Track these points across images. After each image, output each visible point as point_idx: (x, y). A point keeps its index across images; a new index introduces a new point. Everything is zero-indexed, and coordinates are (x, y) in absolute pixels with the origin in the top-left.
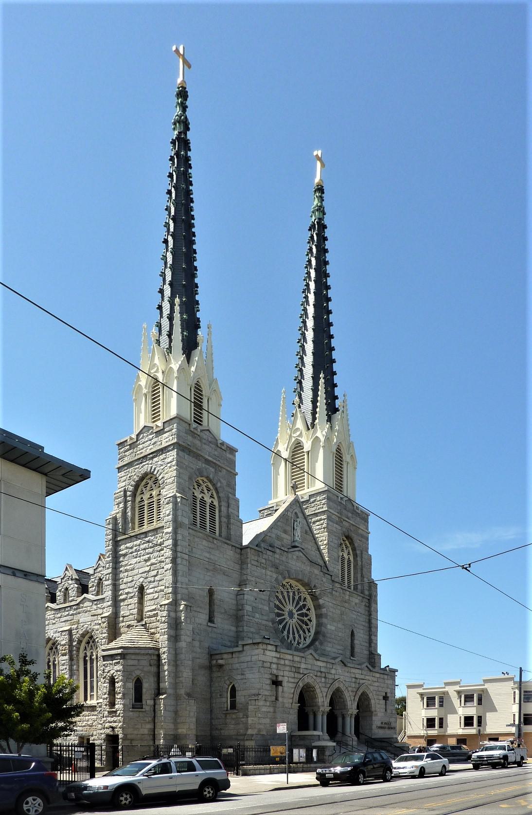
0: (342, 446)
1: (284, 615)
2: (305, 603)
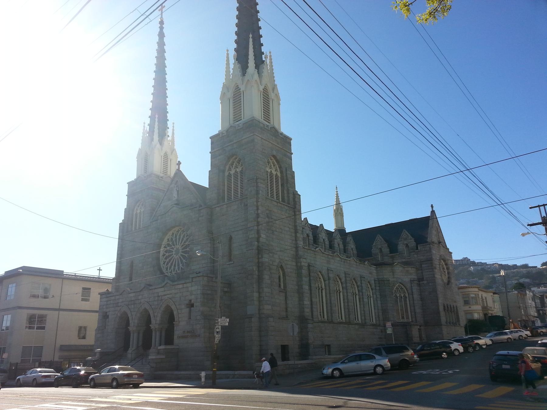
0: (268, 86)
1: (182, 255)
2: (165, 260)
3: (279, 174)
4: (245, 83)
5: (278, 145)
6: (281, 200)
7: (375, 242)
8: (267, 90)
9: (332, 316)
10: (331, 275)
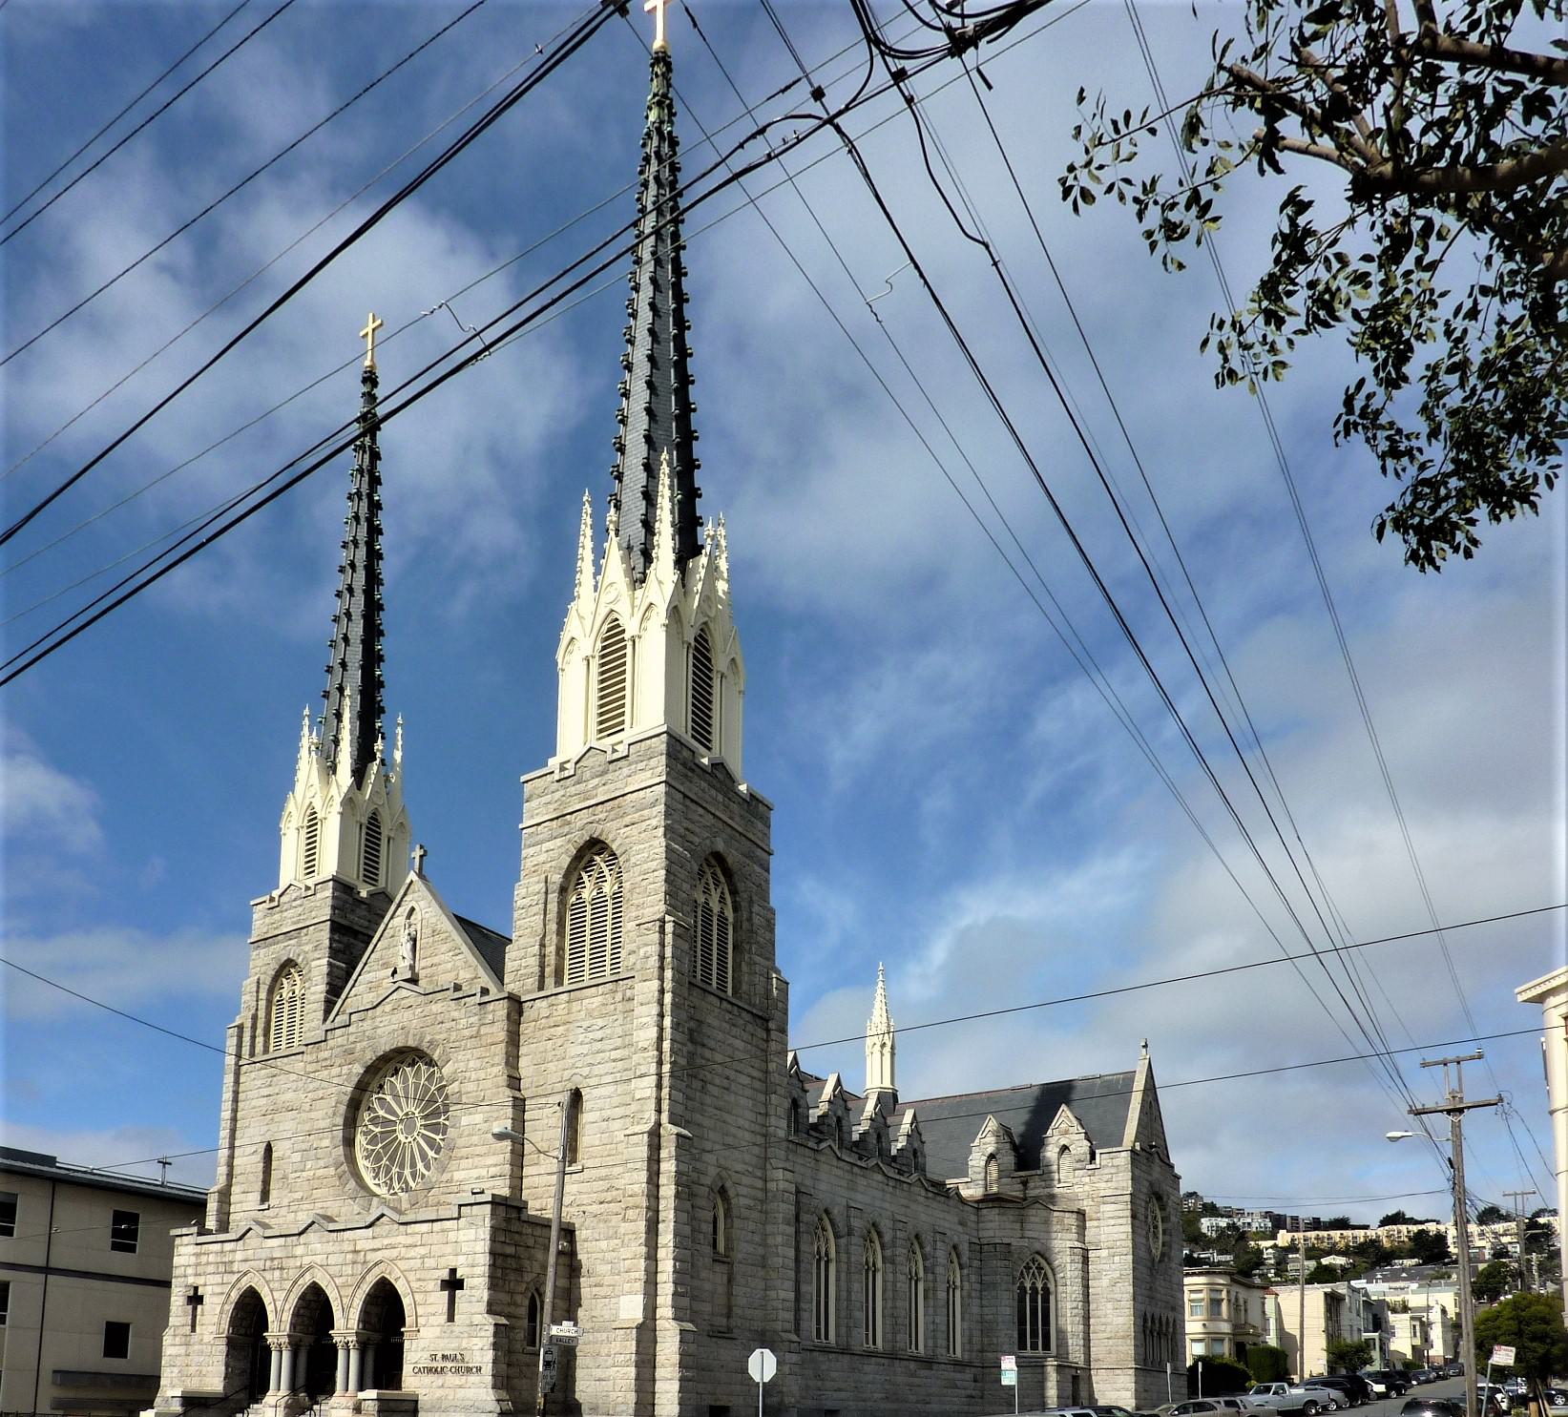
1: (425, 1126)
3: (729, 914)
4: (639, 615)
5: (730, 822)
6: (730, 992)
7: (979, 1136)
8: (706, 641)
9: (849, 1335)
10: (856, 1223)
